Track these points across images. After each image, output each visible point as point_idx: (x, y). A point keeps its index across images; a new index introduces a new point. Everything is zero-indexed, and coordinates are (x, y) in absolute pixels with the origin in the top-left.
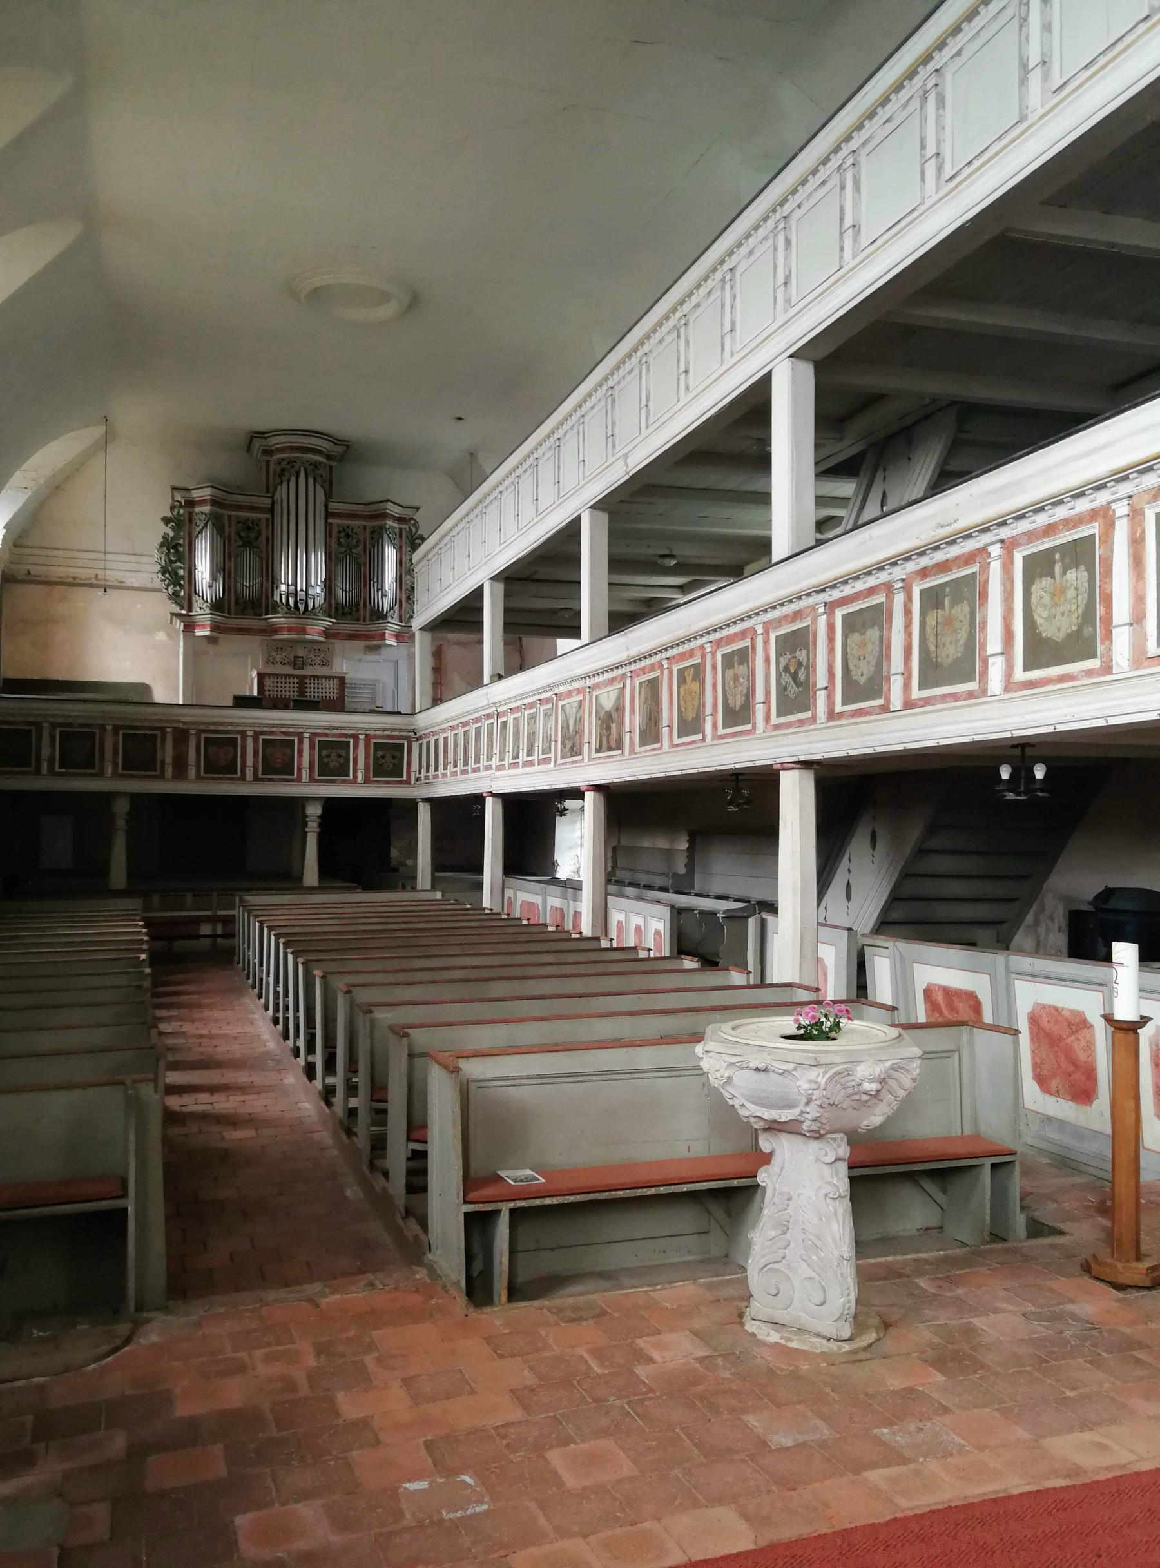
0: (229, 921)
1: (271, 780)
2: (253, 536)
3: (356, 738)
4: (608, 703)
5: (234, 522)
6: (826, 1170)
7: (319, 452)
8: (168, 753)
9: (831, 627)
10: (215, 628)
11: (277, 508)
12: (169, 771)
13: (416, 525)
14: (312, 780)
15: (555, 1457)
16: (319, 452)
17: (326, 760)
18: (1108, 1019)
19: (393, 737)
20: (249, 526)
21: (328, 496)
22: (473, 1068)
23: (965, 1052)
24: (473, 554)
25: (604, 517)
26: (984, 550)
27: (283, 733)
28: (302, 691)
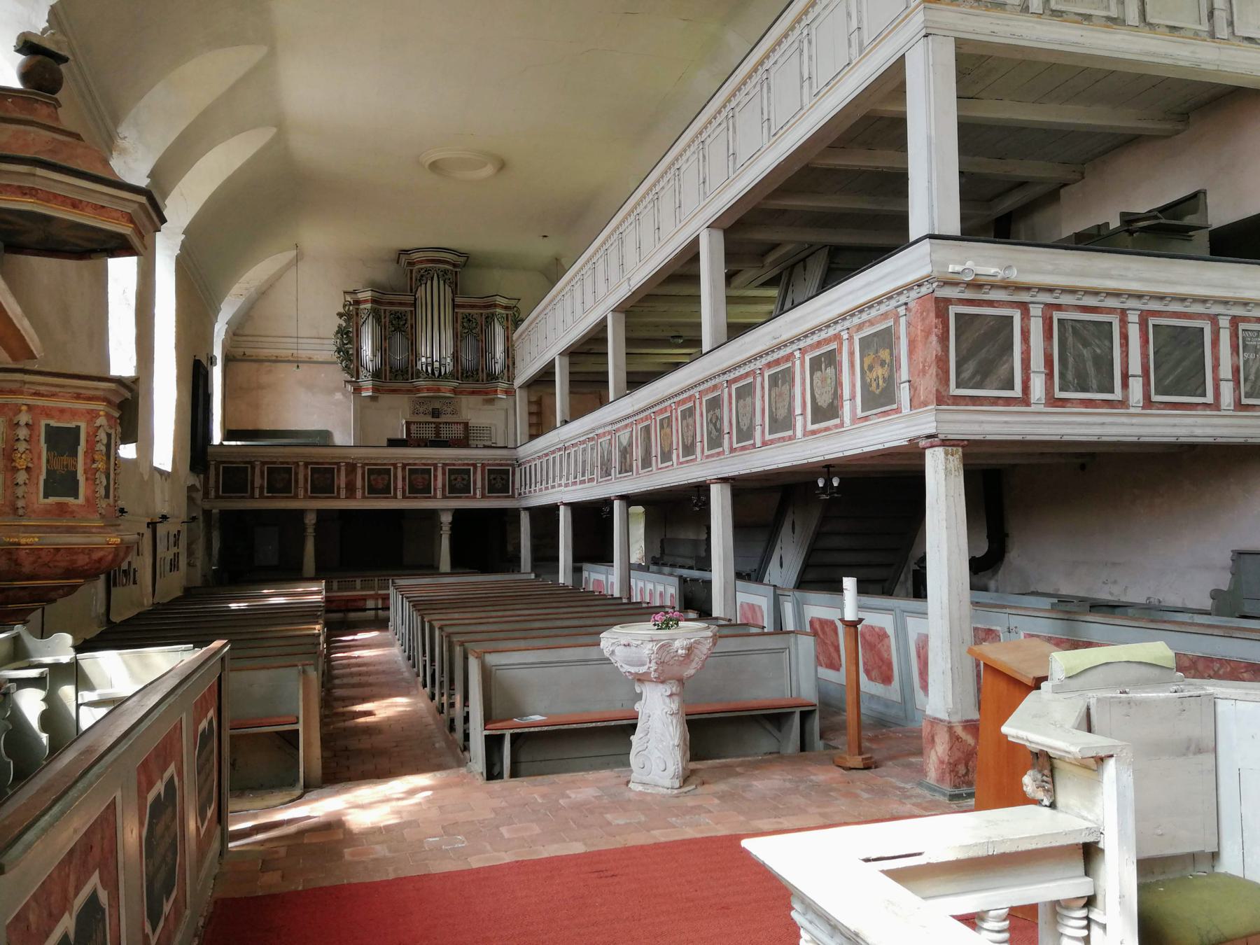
0: (386, 598)
3: (475, 465)
4: (625, 442)
6: (667, 700)
7: (448, 263)
8: (342, 480)
9: (730, 395)
10: (375, 389)
11: (418, 303)
12: (343, 493)
13: (518, 311)
14: (444, 497)
15: (503, 830)
16: (448, 263)
18: (842, 620)
20: (398, 317)
21: (454, 293)
22: (492, 659)
23: (793, 650)
24: (549, 336)
25: (623, 316)
26: (792, 354)
28: (438, 434)
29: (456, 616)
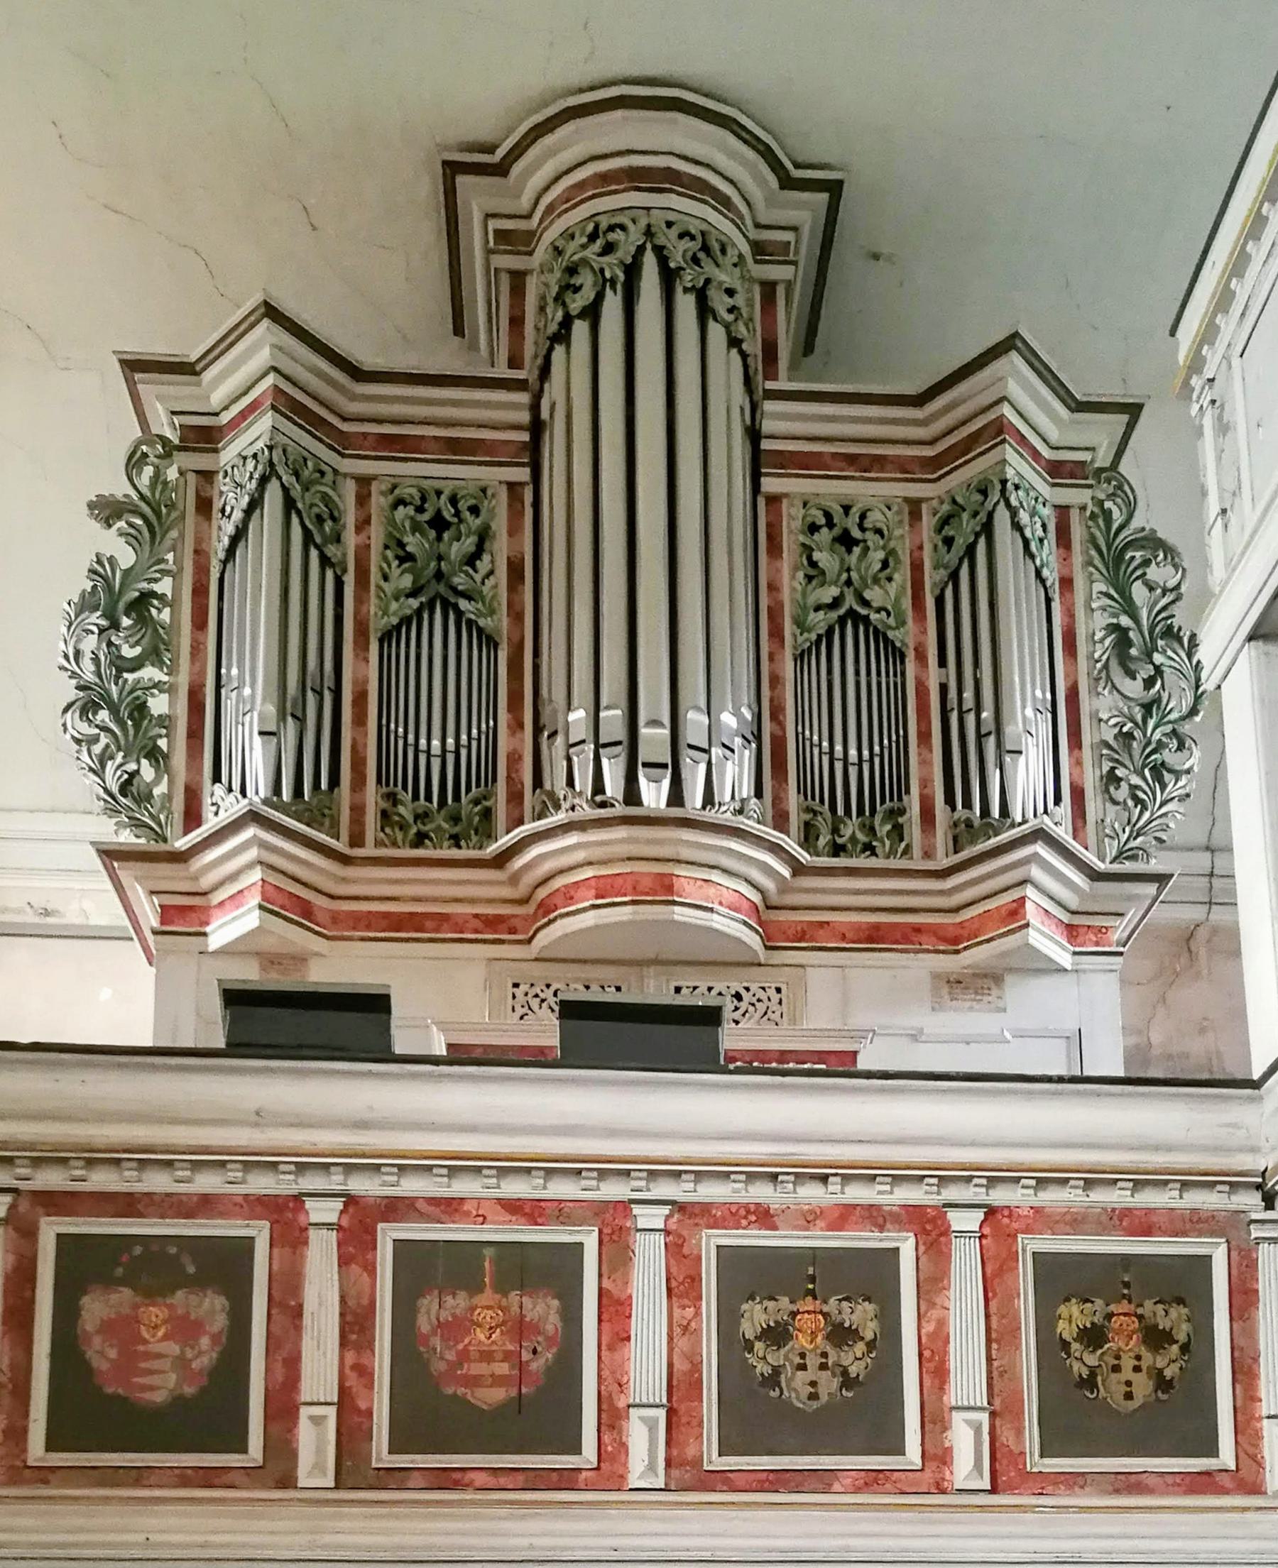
1: (446, 1480)
2: (458, 549)
5: (378, 502)
13: (1122, 490)
17: (762, 1360)
19: (1142, 1224)
27: (514, 1207)
29: (660, 1527)
